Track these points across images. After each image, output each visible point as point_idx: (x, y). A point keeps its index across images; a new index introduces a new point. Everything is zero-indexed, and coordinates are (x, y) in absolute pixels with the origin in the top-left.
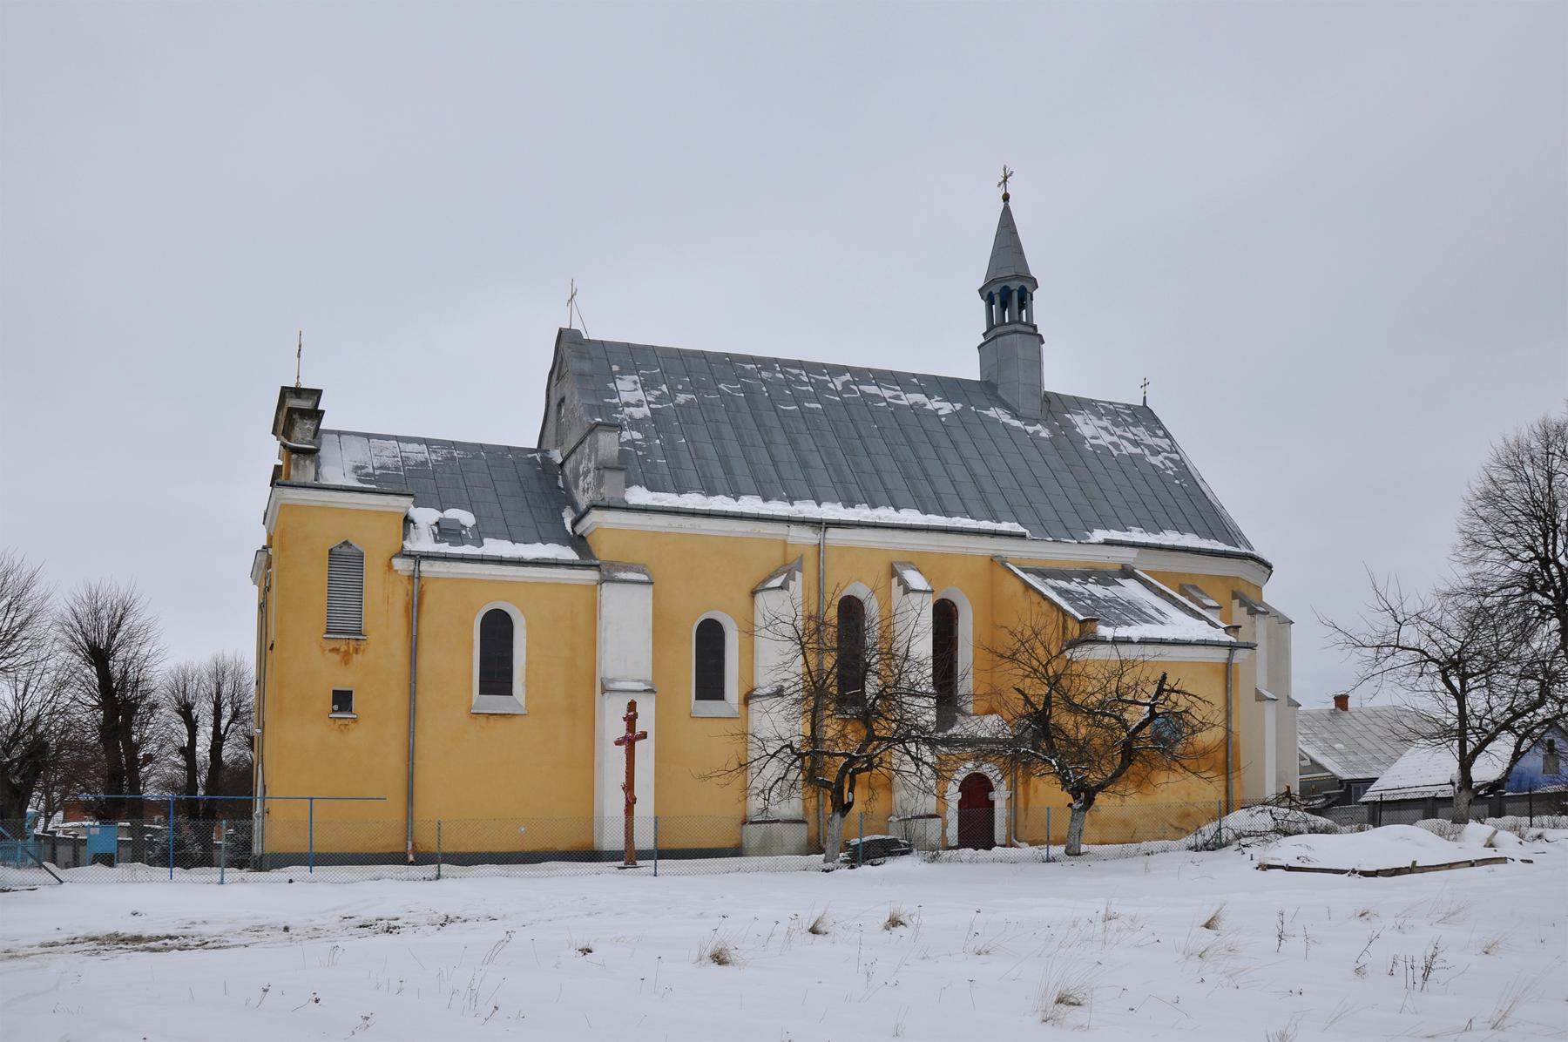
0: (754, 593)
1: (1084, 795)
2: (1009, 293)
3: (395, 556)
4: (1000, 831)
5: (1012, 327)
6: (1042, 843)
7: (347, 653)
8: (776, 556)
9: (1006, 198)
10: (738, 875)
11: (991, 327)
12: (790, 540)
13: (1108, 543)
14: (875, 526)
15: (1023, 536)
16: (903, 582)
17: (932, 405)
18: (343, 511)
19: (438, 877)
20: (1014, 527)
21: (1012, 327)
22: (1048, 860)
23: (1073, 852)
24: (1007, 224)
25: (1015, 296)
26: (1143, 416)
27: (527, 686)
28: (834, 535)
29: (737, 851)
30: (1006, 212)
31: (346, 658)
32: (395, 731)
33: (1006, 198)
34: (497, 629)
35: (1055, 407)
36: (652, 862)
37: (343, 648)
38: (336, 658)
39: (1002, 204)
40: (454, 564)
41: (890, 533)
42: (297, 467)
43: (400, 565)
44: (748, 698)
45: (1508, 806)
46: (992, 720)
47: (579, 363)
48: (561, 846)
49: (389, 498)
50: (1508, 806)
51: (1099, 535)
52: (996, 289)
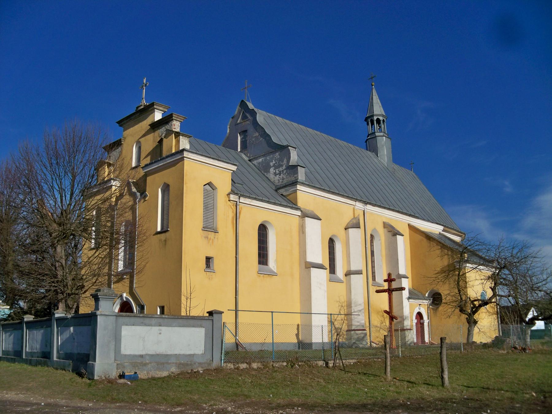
25: (382, 122)
27: (276, 261)
34: (263, 230)
44: (348, 274)
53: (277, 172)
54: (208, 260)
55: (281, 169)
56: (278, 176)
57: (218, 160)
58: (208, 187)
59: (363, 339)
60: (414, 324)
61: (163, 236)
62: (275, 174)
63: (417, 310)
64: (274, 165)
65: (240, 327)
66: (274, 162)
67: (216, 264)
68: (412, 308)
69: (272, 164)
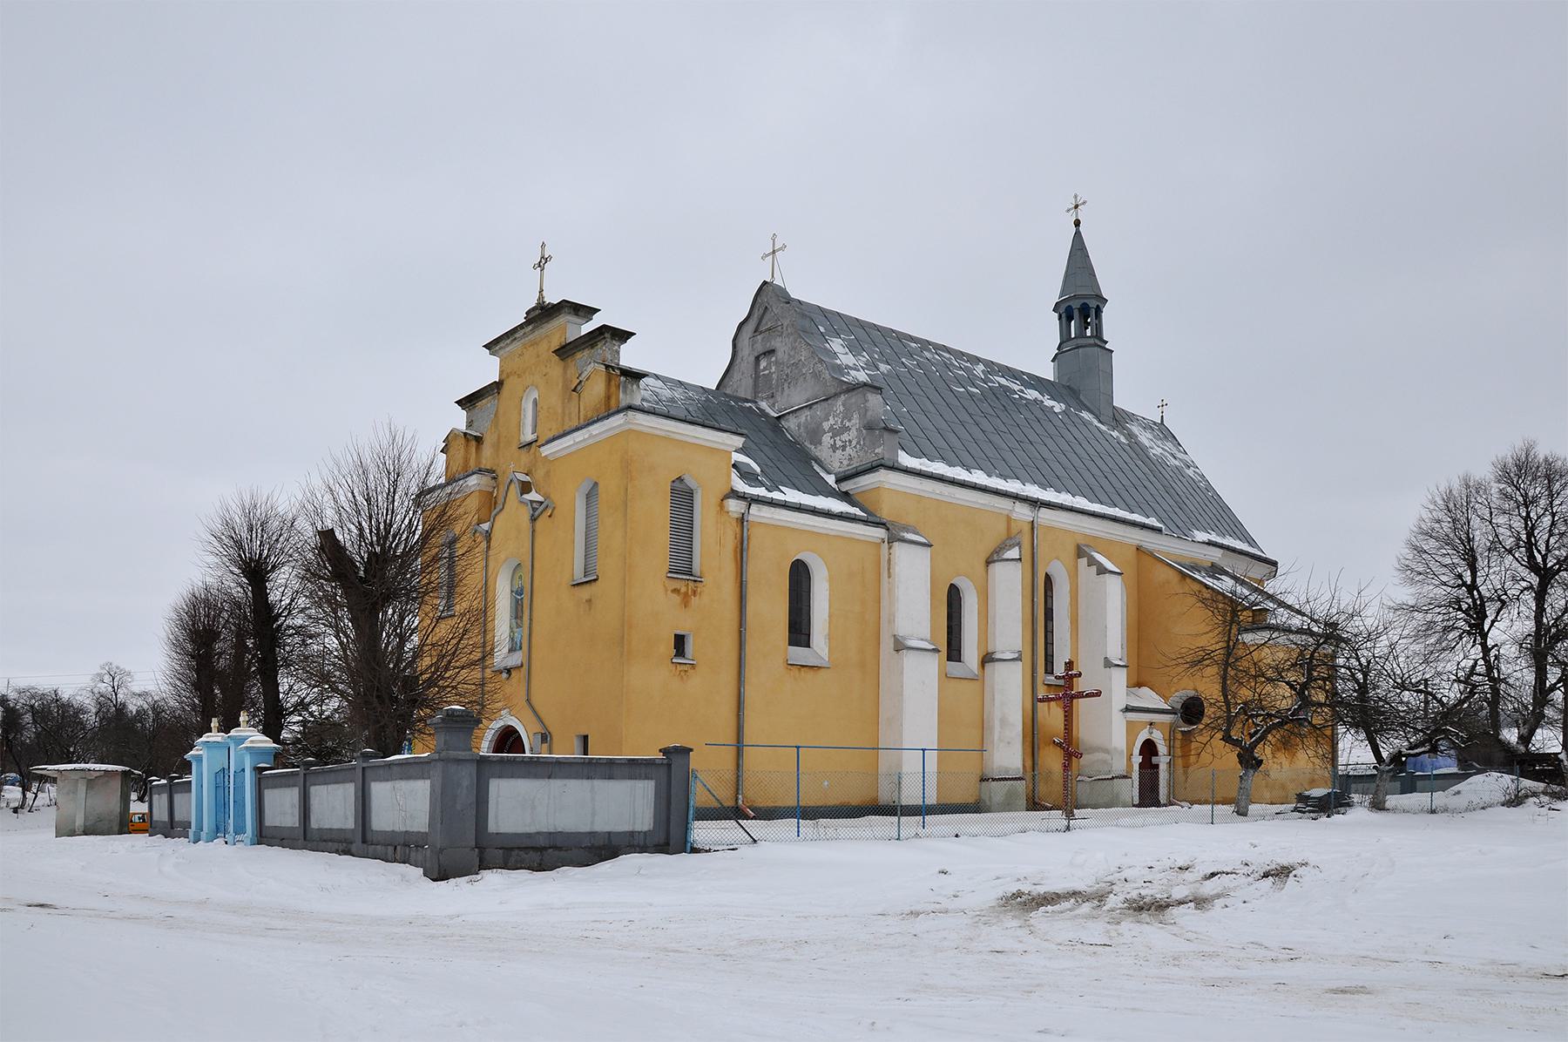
0: (988, 562)
1: (1249, 761)
2: (1081, 309)
3: (727, 497)
4: (1163, 798)
5: (1091, 341)
6: (1206, 802)
7: (686, 594)
8: (998, 531)
9: (1077, 223)
10: (918, 841)
11: (1065, 338)
12: (1014, 516)
13: (1210, 543)
14: (1071, 509)
15: (1159, 530)
16: (1092, 562)
17: (1049, 403)
18: (683, 444)
19: (1068, 828)
20: (1152, 521)
21: (1091, 341)
22: (1433, 812)
23: (1241, 812)
24: (1078, 246)
25: (1093, 312)
26: (1161, 430)
27: (830, 637)
28: (1044, 513)
29: (976, 807)
30: (1078, 235)
31: (686, 603)
32: (728, 676)
33: (1077, 223)
34: (799, 576)
35: (1119, 419)
36: (895, 819)
37: (683, 590)
38: (676, 599)
39: (1074, 229)
40: (778, 510)
41: (1080, 516)
42: (625, 392)
43: (734, 506)
44: (987, 659)
45: (1419, 784)
46: (334, 703)
47: (772, 315)
48: (833, 800)
49: (725, 435)
50: (1419, 784)
51: (1201, 536)
52: (1076, 305)
53: (839, 444)
54: (680, 641)
55: (845, 437)
56: (839, 452)
57: (704, 426)
58: (677, 484)
59: (238, 605)
60: (1136, 767)
61: (585, 592)
62: (834, 448)
63: (1143, 736)
64: (831, 429)
65: (542, 714)
66: (832, 421)
67: (669, 647)
68: (1132, 729)
69: (826, 426)
